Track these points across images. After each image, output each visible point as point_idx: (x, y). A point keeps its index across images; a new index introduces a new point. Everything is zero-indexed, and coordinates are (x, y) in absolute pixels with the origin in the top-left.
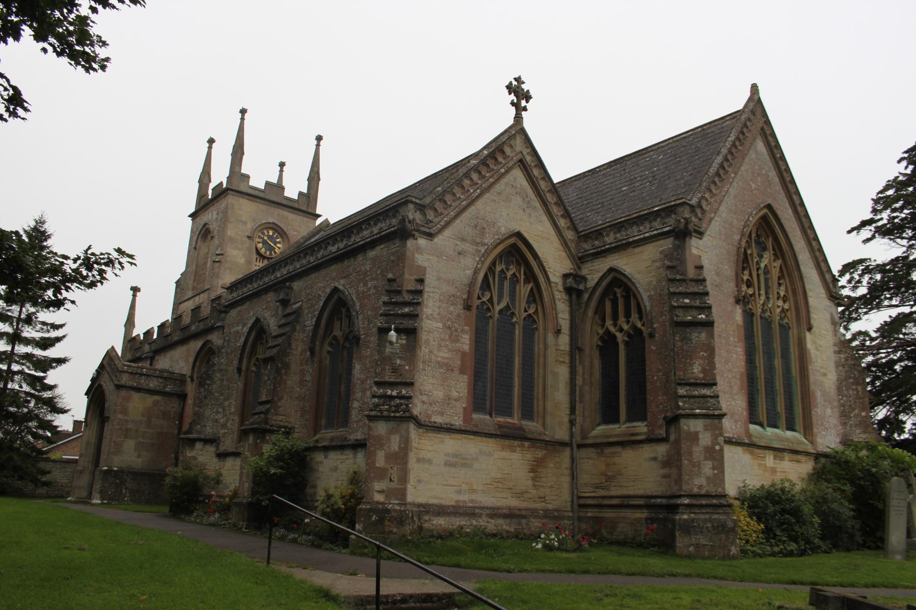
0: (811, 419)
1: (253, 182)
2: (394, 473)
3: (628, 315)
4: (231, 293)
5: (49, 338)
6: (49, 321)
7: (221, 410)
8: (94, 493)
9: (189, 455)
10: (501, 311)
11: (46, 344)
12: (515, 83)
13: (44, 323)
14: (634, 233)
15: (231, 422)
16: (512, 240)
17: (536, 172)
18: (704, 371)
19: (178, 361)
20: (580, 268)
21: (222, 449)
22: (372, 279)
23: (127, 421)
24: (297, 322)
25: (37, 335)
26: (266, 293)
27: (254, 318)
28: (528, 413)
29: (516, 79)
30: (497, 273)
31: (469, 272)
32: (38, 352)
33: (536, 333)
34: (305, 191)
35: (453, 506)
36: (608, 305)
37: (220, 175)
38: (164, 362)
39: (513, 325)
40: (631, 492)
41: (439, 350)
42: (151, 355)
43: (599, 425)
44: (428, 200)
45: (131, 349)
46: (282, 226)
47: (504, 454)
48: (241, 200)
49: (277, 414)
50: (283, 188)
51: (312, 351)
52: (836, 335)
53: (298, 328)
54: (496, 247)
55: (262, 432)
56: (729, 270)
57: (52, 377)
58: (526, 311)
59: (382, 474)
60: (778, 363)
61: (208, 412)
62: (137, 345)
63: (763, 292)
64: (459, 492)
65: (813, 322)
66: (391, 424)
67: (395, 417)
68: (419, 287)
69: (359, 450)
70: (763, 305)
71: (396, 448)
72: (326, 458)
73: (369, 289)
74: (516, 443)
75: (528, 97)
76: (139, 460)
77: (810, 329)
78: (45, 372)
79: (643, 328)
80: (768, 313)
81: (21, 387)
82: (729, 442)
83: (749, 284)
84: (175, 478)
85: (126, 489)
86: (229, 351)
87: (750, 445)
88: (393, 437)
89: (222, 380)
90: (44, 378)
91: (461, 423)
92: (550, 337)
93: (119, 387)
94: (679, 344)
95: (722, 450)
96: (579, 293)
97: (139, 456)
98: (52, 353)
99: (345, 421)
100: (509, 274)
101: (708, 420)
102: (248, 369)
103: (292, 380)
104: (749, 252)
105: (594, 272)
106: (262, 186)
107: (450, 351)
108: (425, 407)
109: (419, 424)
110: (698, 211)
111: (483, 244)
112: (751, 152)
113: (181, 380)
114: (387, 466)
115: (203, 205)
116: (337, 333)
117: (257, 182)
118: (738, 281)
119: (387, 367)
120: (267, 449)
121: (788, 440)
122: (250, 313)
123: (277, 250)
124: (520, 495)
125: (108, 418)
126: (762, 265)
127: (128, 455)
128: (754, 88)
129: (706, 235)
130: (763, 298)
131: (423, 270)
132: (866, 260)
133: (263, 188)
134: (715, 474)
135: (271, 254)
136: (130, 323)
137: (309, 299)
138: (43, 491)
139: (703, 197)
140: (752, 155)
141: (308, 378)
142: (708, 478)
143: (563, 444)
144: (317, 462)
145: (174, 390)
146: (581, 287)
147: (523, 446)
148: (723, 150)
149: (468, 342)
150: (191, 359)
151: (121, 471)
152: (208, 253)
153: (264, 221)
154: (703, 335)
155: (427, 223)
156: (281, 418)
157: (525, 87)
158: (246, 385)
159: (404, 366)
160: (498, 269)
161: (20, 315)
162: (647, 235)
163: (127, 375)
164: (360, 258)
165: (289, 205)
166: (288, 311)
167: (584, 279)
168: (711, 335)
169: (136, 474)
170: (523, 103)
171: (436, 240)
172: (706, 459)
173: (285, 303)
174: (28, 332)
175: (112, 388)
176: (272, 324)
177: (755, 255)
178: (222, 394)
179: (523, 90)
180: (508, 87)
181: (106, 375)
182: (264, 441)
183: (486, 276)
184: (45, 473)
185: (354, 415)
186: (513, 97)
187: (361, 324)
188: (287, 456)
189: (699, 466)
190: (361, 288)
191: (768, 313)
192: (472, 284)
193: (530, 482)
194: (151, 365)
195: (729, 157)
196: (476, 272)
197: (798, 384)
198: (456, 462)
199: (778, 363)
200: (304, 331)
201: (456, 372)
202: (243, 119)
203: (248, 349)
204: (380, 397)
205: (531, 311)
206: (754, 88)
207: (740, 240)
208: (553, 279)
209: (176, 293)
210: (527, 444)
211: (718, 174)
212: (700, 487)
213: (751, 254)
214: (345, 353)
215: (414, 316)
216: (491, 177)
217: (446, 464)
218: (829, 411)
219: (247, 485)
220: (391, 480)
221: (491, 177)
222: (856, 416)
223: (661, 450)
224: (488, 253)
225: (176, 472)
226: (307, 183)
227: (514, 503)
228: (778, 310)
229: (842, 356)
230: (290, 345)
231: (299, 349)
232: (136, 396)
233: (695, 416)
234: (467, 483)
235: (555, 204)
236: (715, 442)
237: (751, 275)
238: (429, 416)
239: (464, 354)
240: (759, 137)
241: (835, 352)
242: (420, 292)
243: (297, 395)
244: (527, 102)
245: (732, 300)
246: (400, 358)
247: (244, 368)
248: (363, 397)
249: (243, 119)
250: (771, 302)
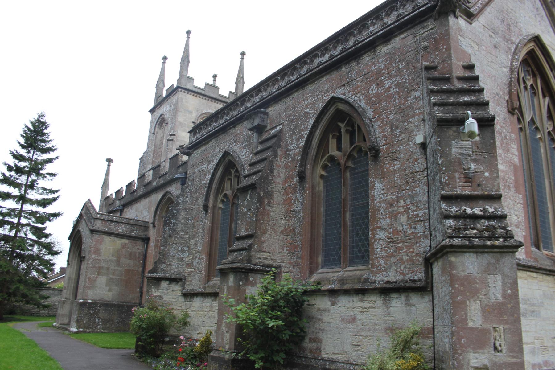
4: (194, 135)
5: (47, 199)
6: (48, 188)
7: (186, 249)
8: (72, 322)
11: (44, 203)
13: (44, 189)
15: (197, 260)
19: (143, 211)
21: (188, 288)
22: (390, 77)
23: (99, 260)
24: (279, 146)
25: (39, 197)
26: (234, 127)
32: (40, 209)
34: (234, 91)
37: (171, 80)
38: (131, 213)
42: (121, 208)
45: (106, 206)
48: (188, 96)
49: (261, 251)
51: (302, 176)
53: (280, 153)
55: (245, 272)
57: (50, 227)
59: (480, 339)
61: (173, 251)
62: (111, 202)
66: (486, 259)
67: (493, 247)
69: (394, 295)
76: (110, 294)
78: (43, 224)
81: (26, 235)
84: (141, 320)
85: (99, 318)
86: (194, 190)
89: (187, 219)
90: (45, 228)
93: (93, 231)
97: (110, 290)
98: (50, 209)
99: (362, 253)
102: (214, 207)
103: (276, 211)
113: (145, 226)
114: (486, 326)
115: (160, 102)
117: (200, 83)
119: (457, 175)
120: (253, 291)
122: (214, 152)
125: (84, 257)
127: (101, 290)
136: (105, 185)
138: (45, 311)
141: (298, 207)
144: (319, 310)
145: (139, 235)
149: (517, 154)
150: (153, 209)
151: (95, 303)
152: (163, 136)
153: (205, 112)
156: (265, 255)
158: (213, 223)
159: (482, 172)
161: (27, 182)
163: (100, 222)
164: (366, 58)
166: (264, 137)
169: (107, 305)
173: (259, 129)
174: (32, 195)
175: (88, 232)
176: (244, 155)
178: (187, 233)
181: (84, 223)
182: (247, 283)
184: (47, 298)
188: (282, 303)
190: (373, 90)
194: (121, 215)
200: (287, 156)
203: (214, 186)
204: (456, 217)
209: (140, 166)
214: (348, 174)
219: (227, 336)
220: (495, 348)
225: (142, 313)
226: (235, 85)
230: (272, 171)
231: (282, 177)
232: (107, 239)
243: (282, 228)
246: (475, 161)
247: (211, 204)
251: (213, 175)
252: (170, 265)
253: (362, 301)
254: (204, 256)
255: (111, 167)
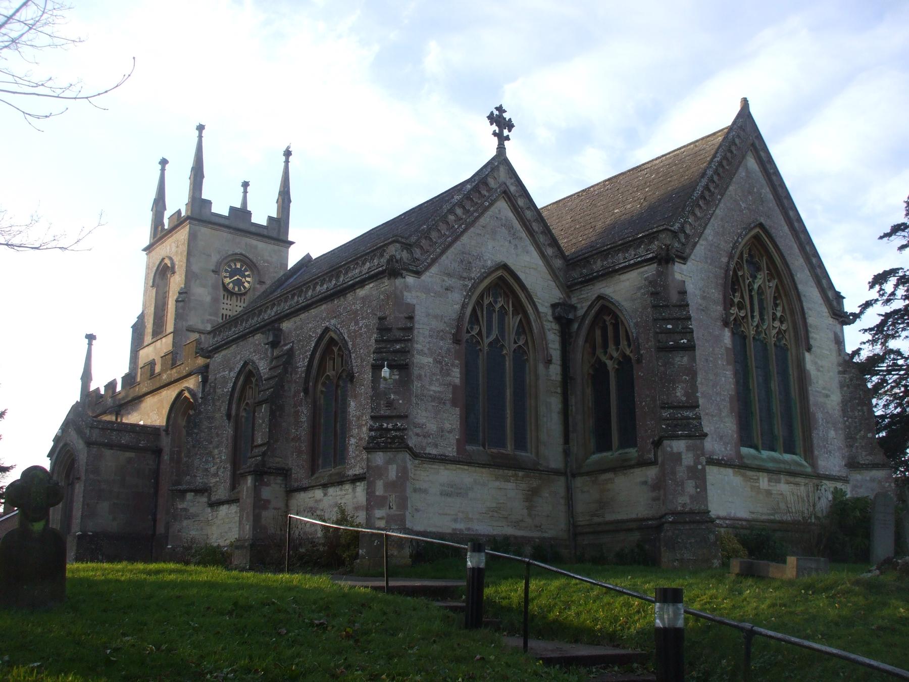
0: (812, 441)
1: (215, 209)
2: (393, 498)
3: (617, 343)
4: (214, 337)
9: (180, 507)
10: (490, 344)
12: (496, 113)
14: (620, 259)
15: (222, 470)
16: (499, 273)
17: (521, 202)
18: (686, 394)
20: (569, 297)
21: (213, 499)
22: (363, 318)
27: (242, 363)
28: (520, 443)
29: (497, 109)
30: (485, 307)
31: (457, 307)
33: (527, 366)
35: (449, 534)
36: (598, 333)
37: (178, 201)
39: (504, 356)
40: (625, 517)
41: (430, 384)
43: (594, 453)
44: (413, 239)
46: (251, 257)
47: (497, 483)
50: (249, 213)
52: (840, 355)
54: (482, 281)
56: (716, 294)
58: (515, 342)
60: (774, 385)
61: (197, 462)
63: (756, 313)
64: (455, 520)
65: (812, 342)
68: (409, 325)
70: (757, 326)
71: (394, 477)
72: (325, 495)
73: (361, 328)
74: (510, 473)
75: (510, 125)
77: (809, 349)
79: (631, 355)
80: (763, 335)
82: (712, 462)
83: (741, 306)
87: (739, 465)
88: (390, 467)
91: (455, 454)
92: (541, 367)
94: (662, 369)
95: (704, 469)
96: (570, 322)
100: (497, 307)
101: (690, 441)
102: (237, 415)
104: (740, 273)
105: (584, 299)
106: (225, 212)
107: (440, 385)
108: (420, 439)
109: (415, 455)
110: (682, 237)
111: (470, 279)
112: (741, 169)
116: (330, 373)
117: (221, 208)
118: (728, 303)
121: (784, 462)
123: (246, 285)
124: (517, 524)
126: (756, 286)
128: (745, 103)
129: (689, 260)
130: (757, 319)
131: (412, 308)
132: (898, 269)
133: (227, 214)
134: (698, 493)
135: (240, 289)
136: (87, 377)
137: (300, 341)
139: (685, 222)
140: (742, 173)
142: (691, 497)
143: (556, 472)
146: (571, 316)
147: (516, 476)
148: (708, 172)
154: (685, 359)
155: (414, 261)
156: (278, 460)
157: (506, 116)
160: (486, 302)
162: (632, 262)
164: (350, 297)
165: (258, 232)
167: (574, 308)
168: (693, 359)
170: (506, 132)
171: (423, 277)
172: (689, 478)
177: (747, 275)
179: (505, 119)
180: (489, 117)
183: (474, 310)
185: (352, 450)
186: (495, 128)
187: (355, 363)
189: (682, 484)
191: (763, 335)
192: (460, 318)
193: (525, 511)
195: (716, 178)
196: (464, 306)
197: (798, 405)
198: (452, 491)
199: (774, 385)
201: (448, 405)
202: (200, 137)
205: (521, 343)
206: (745, 103)
207: (728, 262)
208: (541, 309)
210: (521, 474)
211: (702, 197)
212: (684, 505)
213: (743, 276)
215: (405, 352)
216: (475, 211)
217: (443, 494)
218: (832, 433)
220: (390, 508)
221: (475, 211)
222: (865, 437)
223: (651, 473)
224: (474, 287)
227: (509, 531)
228: (774, 332)
229: (847, 376)
230: (283, 387)
232: (108, 453)
233: (678, 437)
234: (463, 512)
235: (542, 233)
236: (697, 462)
237: (742, 297)
238: (424, 448)
239: (455, 387)
240: (750, 153)
241: (840, 373)
242: (410, 329)
244: (510, 131)
245: (719, 323)
246: (395, 393)
247: (233, 412)
248: (359, 431)
249: (200, 137)
250: (766, 324)
251: (235, 383)
252: (195, 476)
253: (341, 490)
254: (228, 465)
255: (93, 347)
